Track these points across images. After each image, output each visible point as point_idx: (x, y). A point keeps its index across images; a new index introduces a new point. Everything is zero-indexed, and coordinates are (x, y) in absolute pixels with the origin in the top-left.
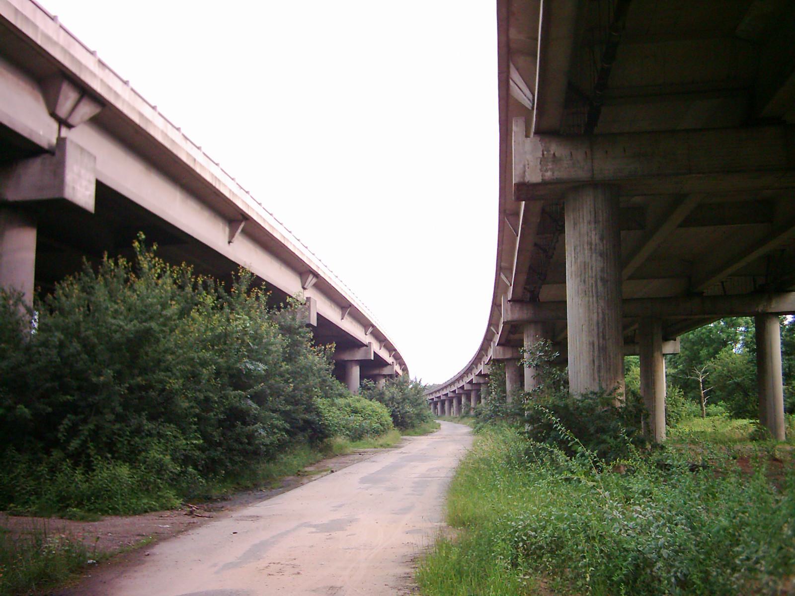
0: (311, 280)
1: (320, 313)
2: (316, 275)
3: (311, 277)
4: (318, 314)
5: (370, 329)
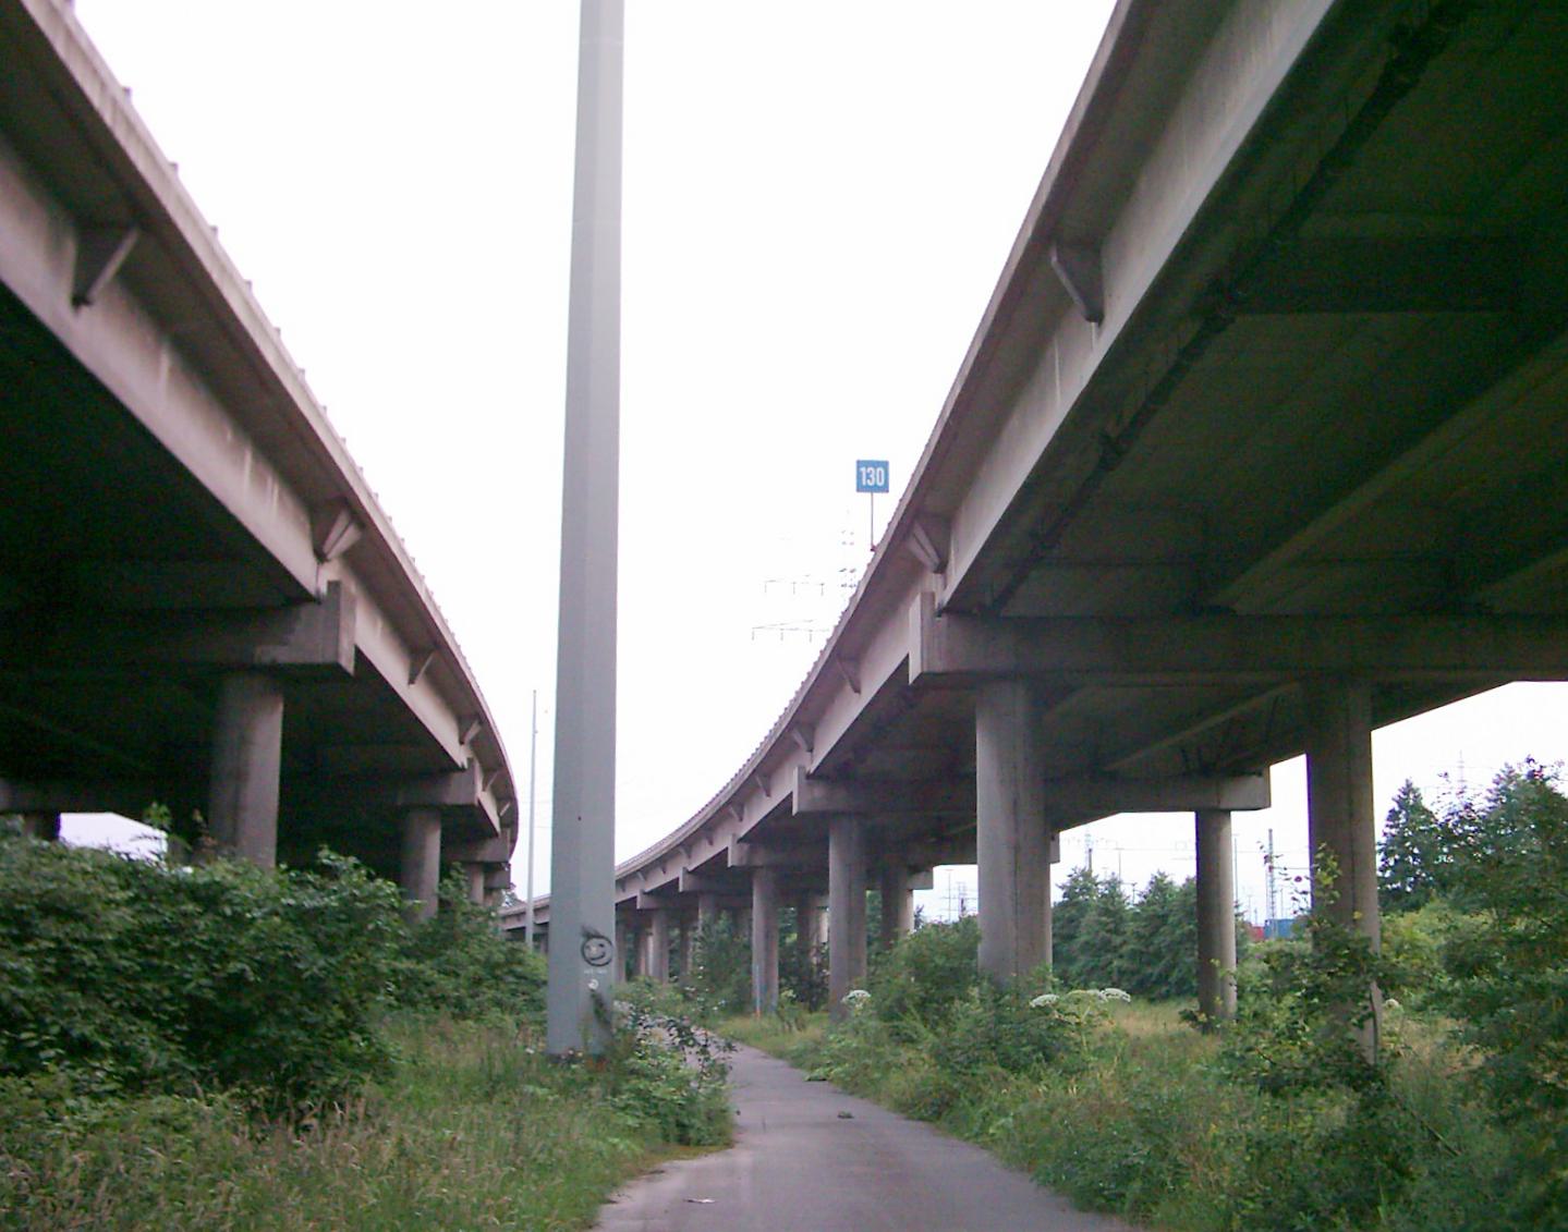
2: (362, 519)
3: (343, 520)
5: (472, 733)
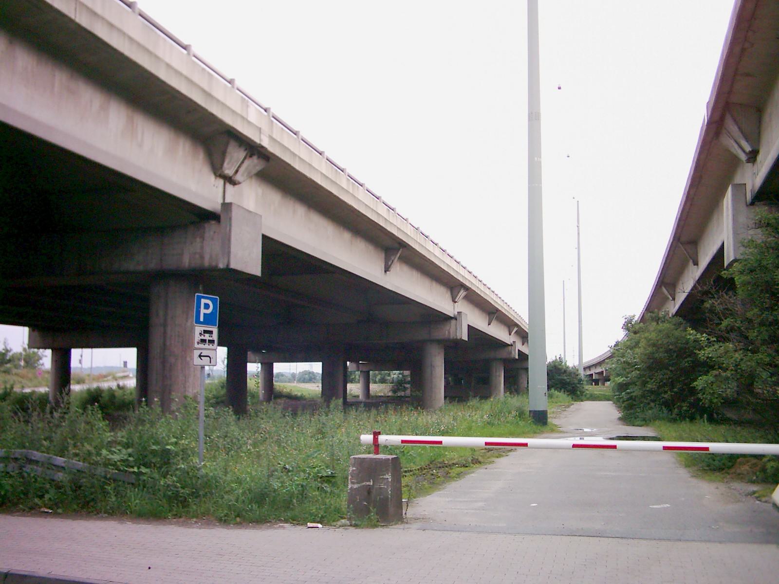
0: (462, 293)
1: (520, 349)
2: (467, 288)
4: (264, 237)
5: (462, 293)
